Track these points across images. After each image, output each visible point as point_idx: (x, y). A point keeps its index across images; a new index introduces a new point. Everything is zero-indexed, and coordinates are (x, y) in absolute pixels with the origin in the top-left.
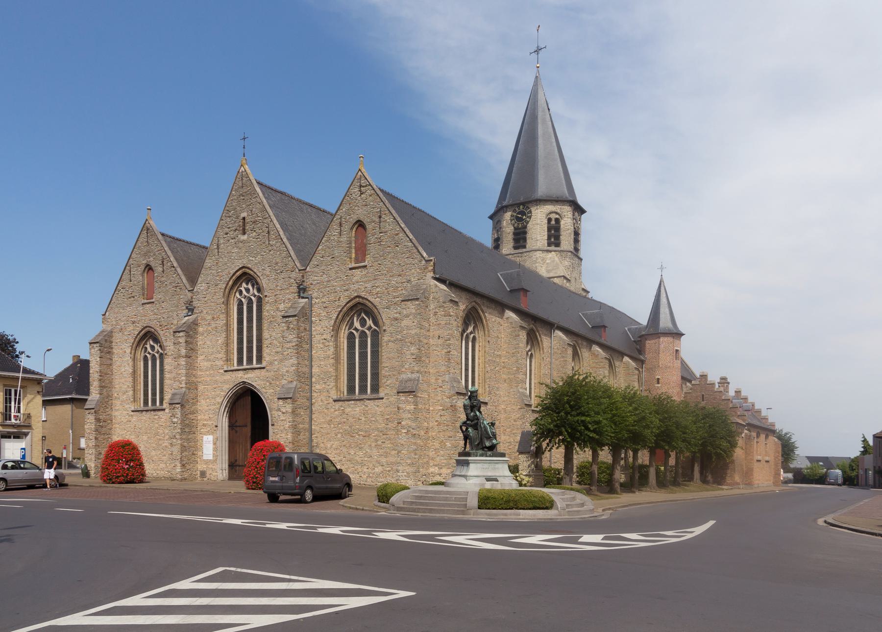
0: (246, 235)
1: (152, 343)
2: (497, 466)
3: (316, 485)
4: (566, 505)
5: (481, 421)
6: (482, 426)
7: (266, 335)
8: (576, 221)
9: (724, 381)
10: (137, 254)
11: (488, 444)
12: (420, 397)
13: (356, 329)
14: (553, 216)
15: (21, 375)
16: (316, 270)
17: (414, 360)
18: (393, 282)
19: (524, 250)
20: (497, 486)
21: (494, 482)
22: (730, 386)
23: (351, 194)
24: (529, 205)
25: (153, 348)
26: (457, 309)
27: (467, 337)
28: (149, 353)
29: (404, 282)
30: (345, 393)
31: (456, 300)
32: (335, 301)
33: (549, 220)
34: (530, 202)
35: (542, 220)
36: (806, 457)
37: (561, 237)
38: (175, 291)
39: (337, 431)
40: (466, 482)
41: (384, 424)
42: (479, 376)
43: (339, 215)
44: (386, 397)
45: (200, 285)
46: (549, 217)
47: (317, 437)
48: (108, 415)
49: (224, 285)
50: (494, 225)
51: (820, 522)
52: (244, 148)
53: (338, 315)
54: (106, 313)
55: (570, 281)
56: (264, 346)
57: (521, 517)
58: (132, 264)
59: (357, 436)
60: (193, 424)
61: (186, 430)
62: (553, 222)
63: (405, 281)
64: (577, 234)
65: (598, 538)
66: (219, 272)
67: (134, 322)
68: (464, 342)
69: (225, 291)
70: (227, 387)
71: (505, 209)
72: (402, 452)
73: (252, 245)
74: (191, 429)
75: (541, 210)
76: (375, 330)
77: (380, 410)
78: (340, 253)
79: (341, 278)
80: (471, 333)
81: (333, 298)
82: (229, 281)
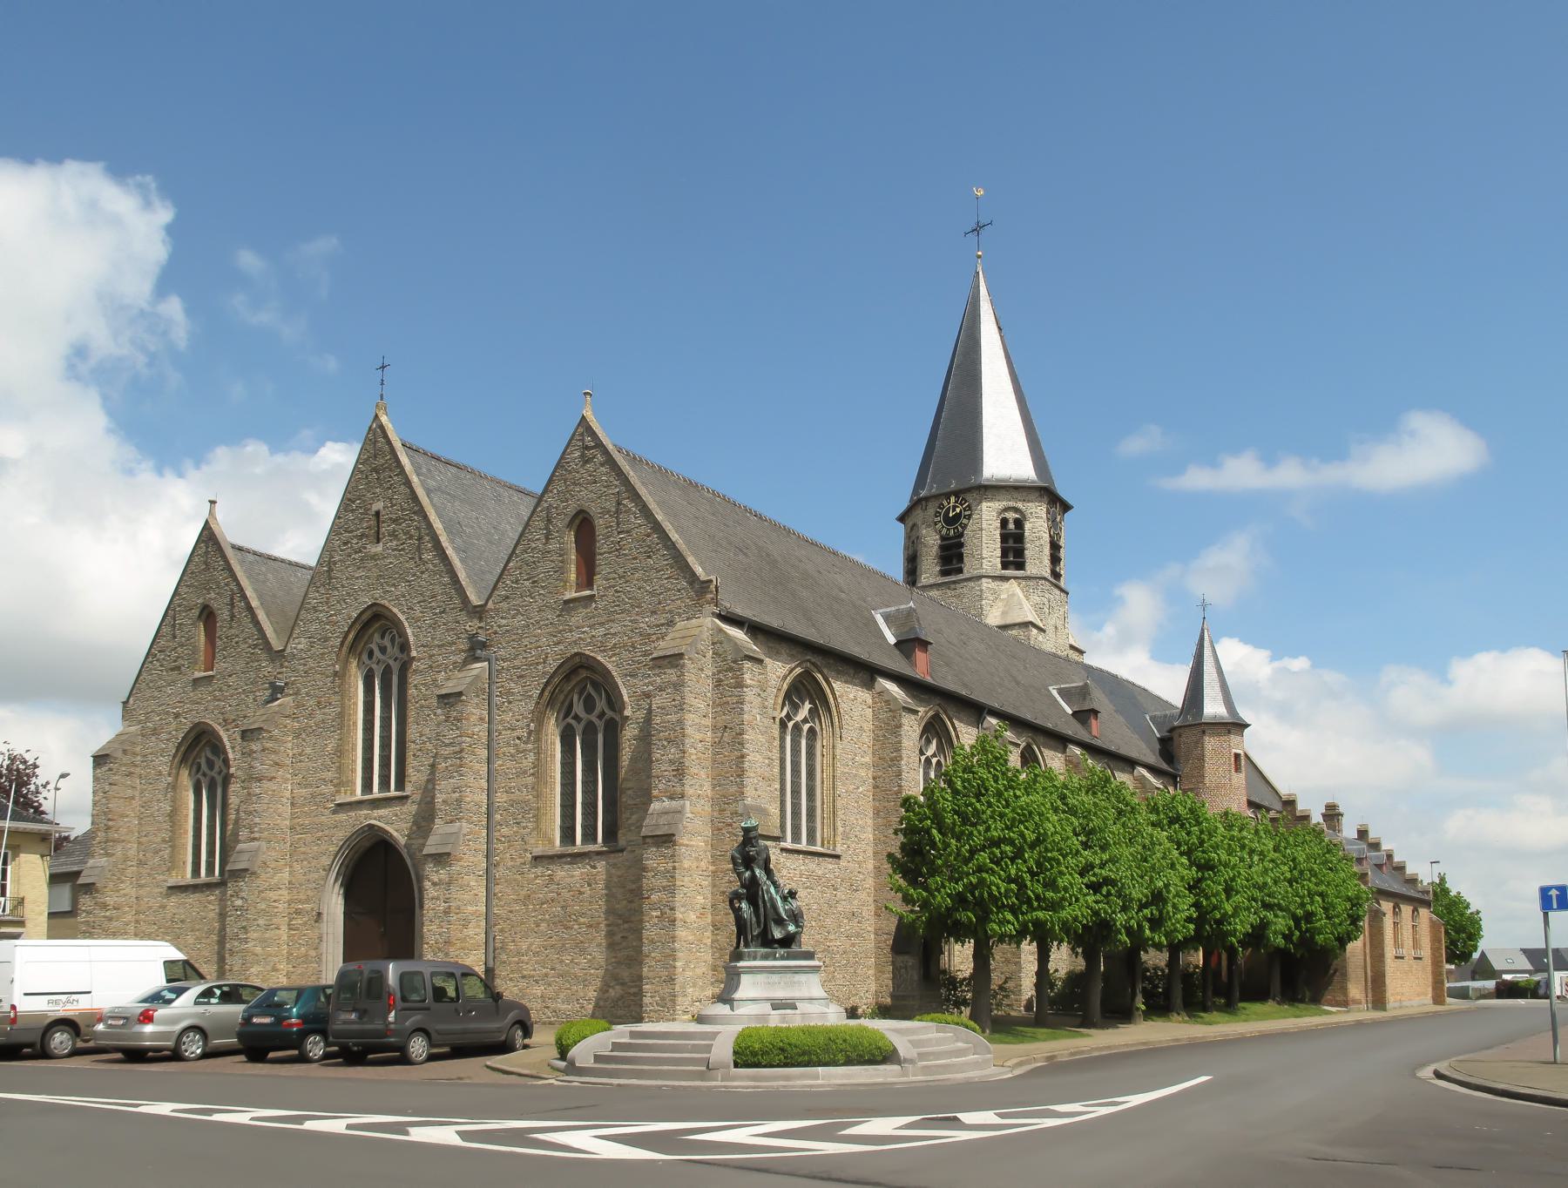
0: (381, 544)
1: (210, 755)
2: (798, 977)
3: (436, 1027)
4: (918, 1054)
5: (765, 888)
6: (766, 898)
7: (412, 732)
8: (1054, 524)
9: (1332, 815)
10: (187, 586)
11: (778, 934)
12: (687, 846)
13: (576, 717)
14: (1011, 516)
15: (7, 826)
16: (504, 605)
17: (675, 773)
18: (642, 625)
19: (961, 577)
20: (794, 1020)
21: (789, 1011)
22: (1344, 820)
23: (568, 463)
24: (968, 496)
25: (211, 765)
26: (760, 674)
27: (797, 727)
28: (204, 775)
29: (663, 625)
30: (558, 842)
31: (762, 657)
32: (537, 664)
33: (1004, 522)
34: (969, 490)
35: (991, 522)
36: (1521, 950)
37: (1026, 552)
38: (253, 653)
39: (540, 917)
40: (732, 1013)
41: (625, 902)
42: (823, 804)
43: (546, 501)
44: (629, 848)
45: (297, 641)
46: (1003, 516)
47: (502, 931)
48: (125, 895)
49: (339, 640)
50: (906, 533)
51: (1427, 1072)
52: (382, 384)
53: (543, 690)
54: (128, 698)
55: (1044, 631)
56: (409, 754)
57: (820, 1082)
58: (179, 606)
59: (576, 927)
60: (276, 910)
61: (259, 922)
62: (1011, 526)
63: (663, 621)
64: (1055, 546)
65: (989, 1117)
66: (331, 615)
67: (177, 716)
68: (788, 739)
69: (340, 650)
70: (341, 835)
71: (924, 503)
72: (653, 955)
73: (391, 563)
74: (271, 920)
75: (989, 504)
76: (612, 719)
77: (619, 873)
78: (549, 571)
79: (548, 619)
80: (805, 721)
81: (534, 658)
82: (349, 631)
